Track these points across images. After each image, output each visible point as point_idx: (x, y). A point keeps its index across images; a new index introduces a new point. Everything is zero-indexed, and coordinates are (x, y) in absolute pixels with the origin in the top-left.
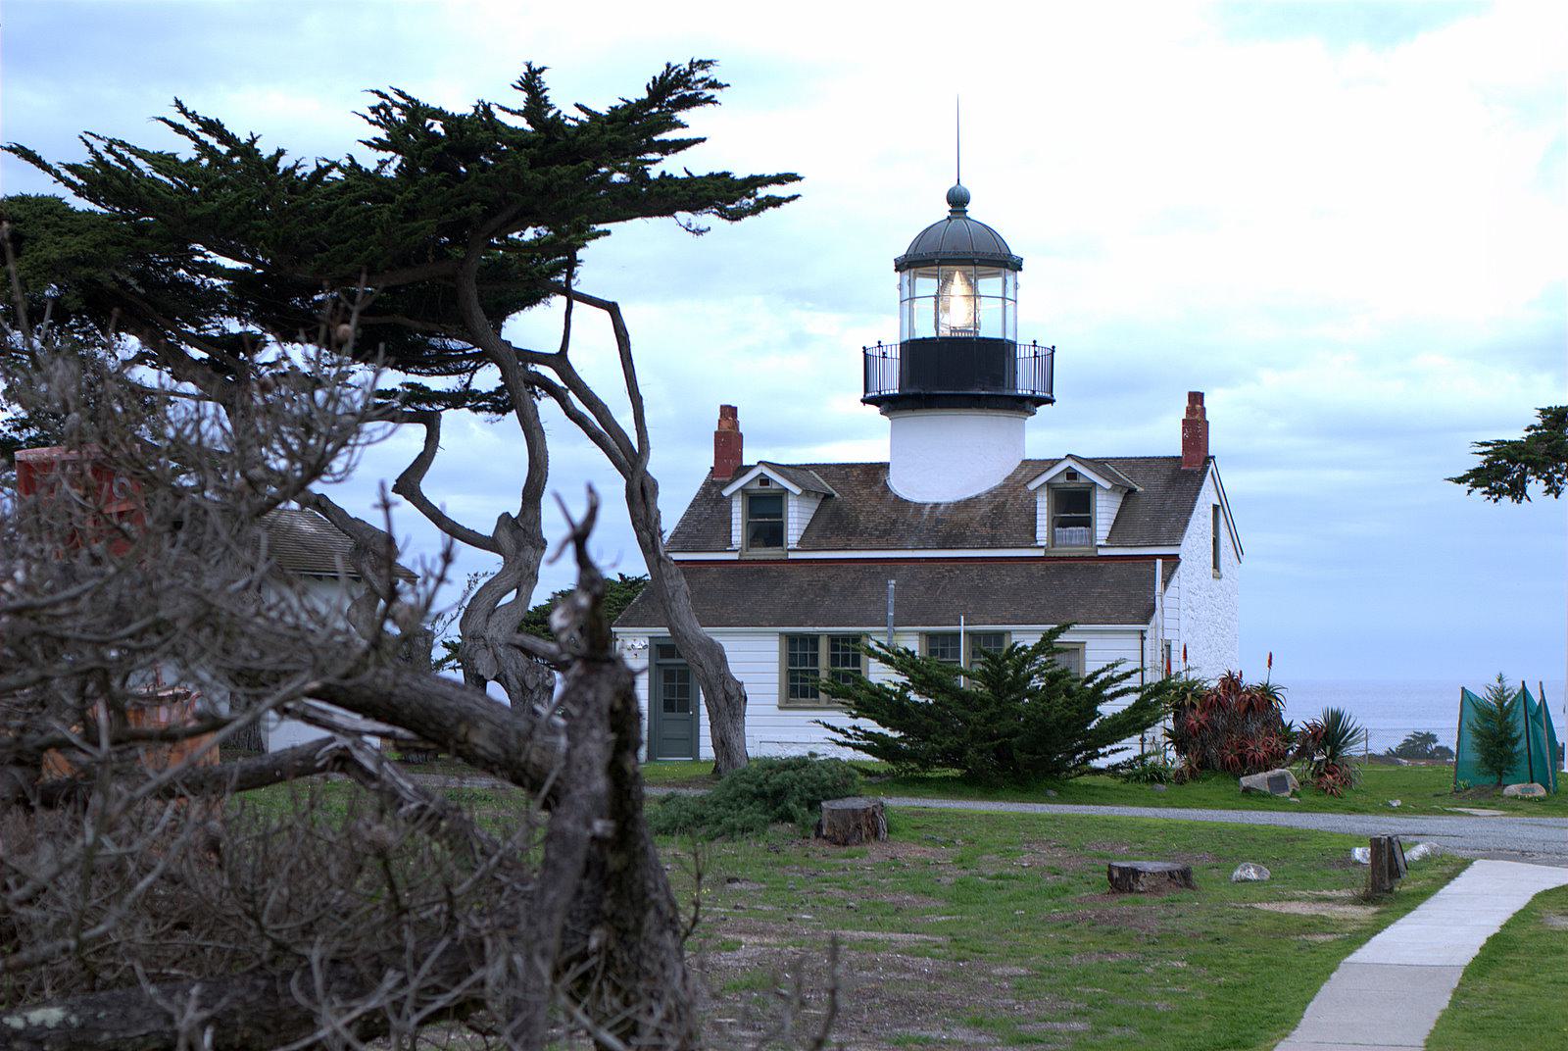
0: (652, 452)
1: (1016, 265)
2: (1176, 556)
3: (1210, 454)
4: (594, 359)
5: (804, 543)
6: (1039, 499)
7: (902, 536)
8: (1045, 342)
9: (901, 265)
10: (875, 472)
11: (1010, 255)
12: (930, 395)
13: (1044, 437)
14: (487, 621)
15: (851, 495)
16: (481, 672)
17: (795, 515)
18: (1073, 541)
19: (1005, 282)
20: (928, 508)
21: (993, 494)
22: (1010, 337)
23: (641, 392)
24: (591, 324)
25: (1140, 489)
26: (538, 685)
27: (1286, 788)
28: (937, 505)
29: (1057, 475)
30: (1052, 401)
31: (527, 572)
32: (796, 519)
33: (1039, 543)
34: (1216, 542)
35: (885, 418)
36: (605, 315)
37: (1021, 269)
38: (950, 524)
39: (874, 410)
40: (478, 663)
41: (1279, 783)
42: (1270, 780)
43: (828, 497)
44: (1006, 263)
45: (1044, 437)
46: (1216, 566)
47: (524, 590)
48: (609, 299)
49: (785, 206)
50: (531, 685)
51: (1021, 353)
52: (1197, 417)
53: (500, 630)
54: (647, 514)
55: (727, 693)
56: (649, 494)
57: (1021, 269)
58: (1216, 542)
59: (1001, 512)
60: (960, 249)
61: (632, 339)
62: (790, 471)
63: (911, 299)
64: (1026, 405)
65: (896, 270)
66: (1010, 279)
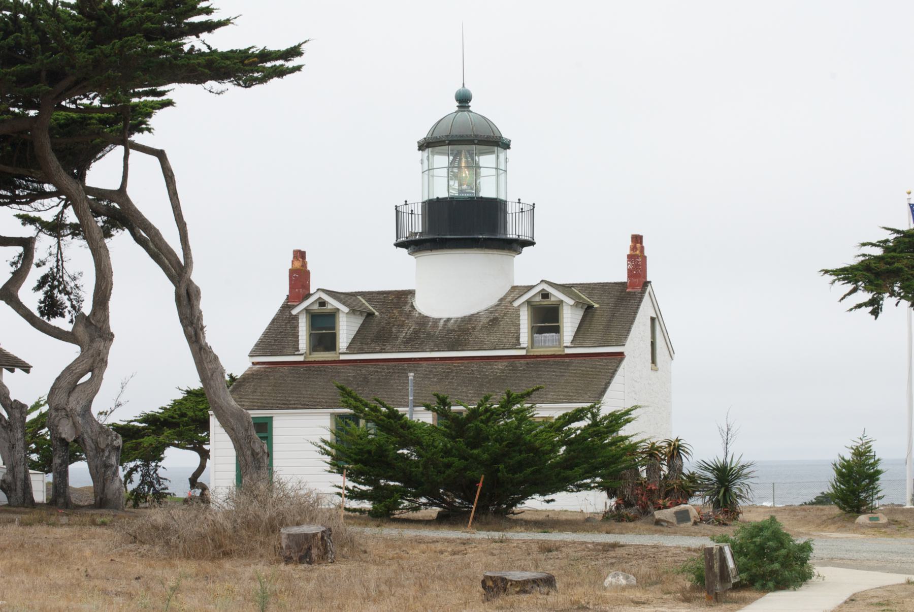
0: (194, 265)
1: (506, 146)
2: (621, 355)
3: (648, 280)
4: (148, 198)
5: (351, 348)
6: (521, 313)
7: (423, 342)
8: (527, 200)
9: (425, 145)
10: (403, 298)
11: (501, 137)
12: (442, 239)
13: (526, 269)
14: (69, 396)
15: (386, 313)
16: (63, 436)
17: (345, 327)
18: (547, 344)
19: (498, 157)
20: (442, 322)
21: (490, 311)
22: (502, 197)
23: (185, 219)
24: (145, 169)
25: (596, 306)
26: (107, 445)
27: (688, 519)
28: (449, 320)
29: (534, 296)
30: (531, 243)
31: (98, 359)
32: (346, 329)
33: (522, 346)
34: (653, 344)
35: (412, 257)
36: (155, 160)
37: (509, 148)
38: (461, 332)
39: (404, 251)
40: (61, 429)
41: (683, 517)
42: (676, 513)
43: (370, 315)
44: (495, 142)
45: (526, 269)
46: (653, 361)
47: (96, 371)
48: (158, 147)
49: (288, 77)
50: (102, 446)
51: (512, 208)
52: (638, 252)
53: (78, 403)
54: (192, 314)
55: (253, 450)
56: (194, 298)
57: (509, 148)
58: (653, 344)
59: (497, 320)
60: (466, 137)
61: (176, 178)
62: (342, 296)
63: (429, 170)
64: (517, 245)
65: (419, 149)
66: (502, 156)
